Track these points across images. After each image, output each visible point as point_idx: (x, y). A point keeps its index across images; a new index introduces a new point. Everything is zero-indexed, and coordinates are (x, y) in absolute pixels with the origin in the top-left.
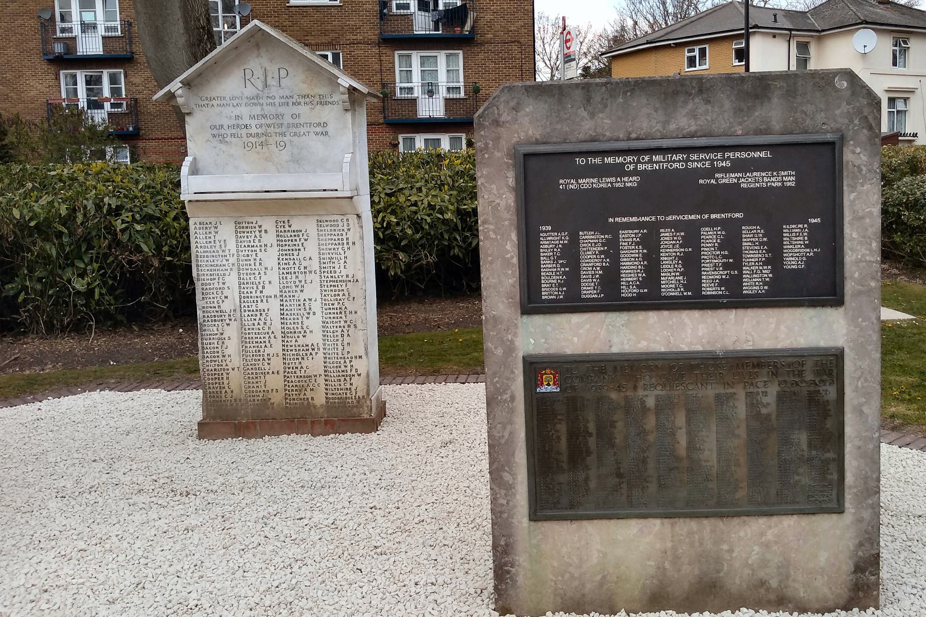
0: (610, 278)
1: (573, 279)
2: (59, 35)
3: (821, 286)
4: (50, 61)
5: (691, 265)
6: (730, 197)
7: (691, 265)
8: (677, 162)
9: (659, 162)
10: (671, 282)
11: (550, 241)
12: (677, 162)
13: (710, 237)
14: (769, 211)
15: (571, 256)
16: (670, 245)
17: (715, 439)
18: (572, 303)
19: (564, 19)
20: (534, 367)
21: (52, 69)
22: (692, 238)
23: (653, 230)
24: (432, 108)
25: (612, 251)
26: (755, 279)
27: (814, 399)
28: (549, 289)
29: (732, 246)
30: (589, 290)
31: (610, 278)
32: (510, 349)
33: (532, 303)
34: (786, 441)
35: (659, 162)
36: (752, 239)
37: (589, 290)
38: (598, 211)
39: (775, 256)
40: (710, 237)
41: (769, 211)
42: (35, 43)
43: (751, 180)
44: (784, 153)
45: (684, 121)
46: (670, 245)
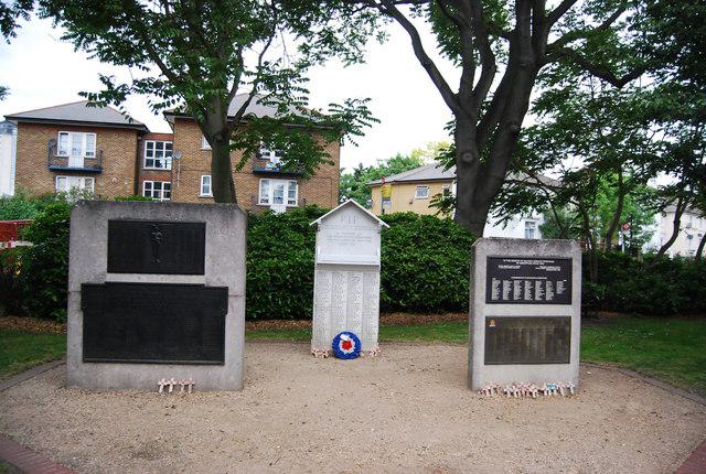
0: (511, 294)
1: (501, 295)
2: (59, 155)
3: (565, 299)
4: (52, 170)
5: (533, 291)
6: (544, 273)
7: (533, 291)
8: (530, 262)
9: (526, 262)
10: (527, 296)
11: (495, 283)
12: (530, 262)
13: (538, 284)
14: (553, 277)
15: (501, 287)
16: (528, 285)
17: (536, 343)
18: (500, 301)
19: (363, 135)
20: (488, 320)
21: (52, 174)
22: (522, 285)
23: (523, 281)
24: (77, 162)
25: (512, 286)
26: (549, 297)
27: (563, 330)
28: (494, 296)
29: (543, 286)
30: (505, 297)
31: (511, 294)
32: (482, 314)
33: (489, 300)
34: (555, 342)
35: (526, 262)
36: (549, 283)
37: (505, 297)
38: (507, 275)
39: (554, 291)
40: (538, 284)
41: (553, 277)
42: (44, 159)
43: (549, 269)
44: (558, 261)
45: (531, 253)
46: (528, 285)
